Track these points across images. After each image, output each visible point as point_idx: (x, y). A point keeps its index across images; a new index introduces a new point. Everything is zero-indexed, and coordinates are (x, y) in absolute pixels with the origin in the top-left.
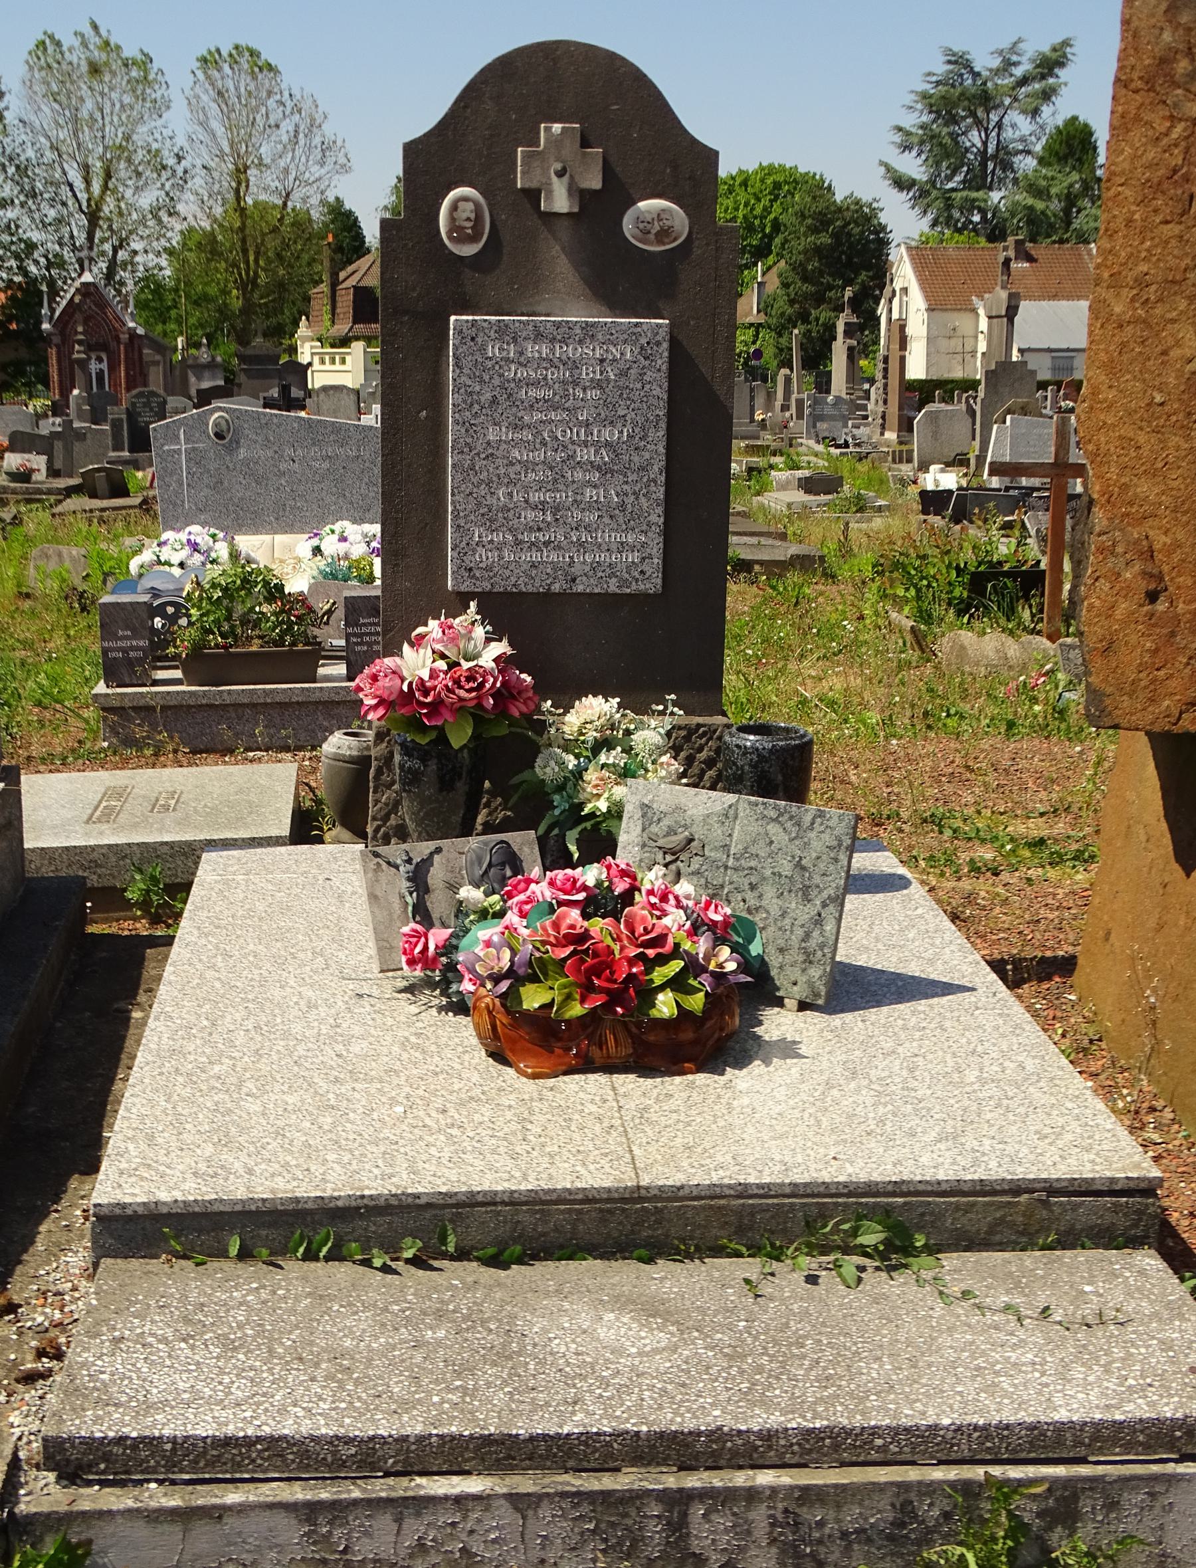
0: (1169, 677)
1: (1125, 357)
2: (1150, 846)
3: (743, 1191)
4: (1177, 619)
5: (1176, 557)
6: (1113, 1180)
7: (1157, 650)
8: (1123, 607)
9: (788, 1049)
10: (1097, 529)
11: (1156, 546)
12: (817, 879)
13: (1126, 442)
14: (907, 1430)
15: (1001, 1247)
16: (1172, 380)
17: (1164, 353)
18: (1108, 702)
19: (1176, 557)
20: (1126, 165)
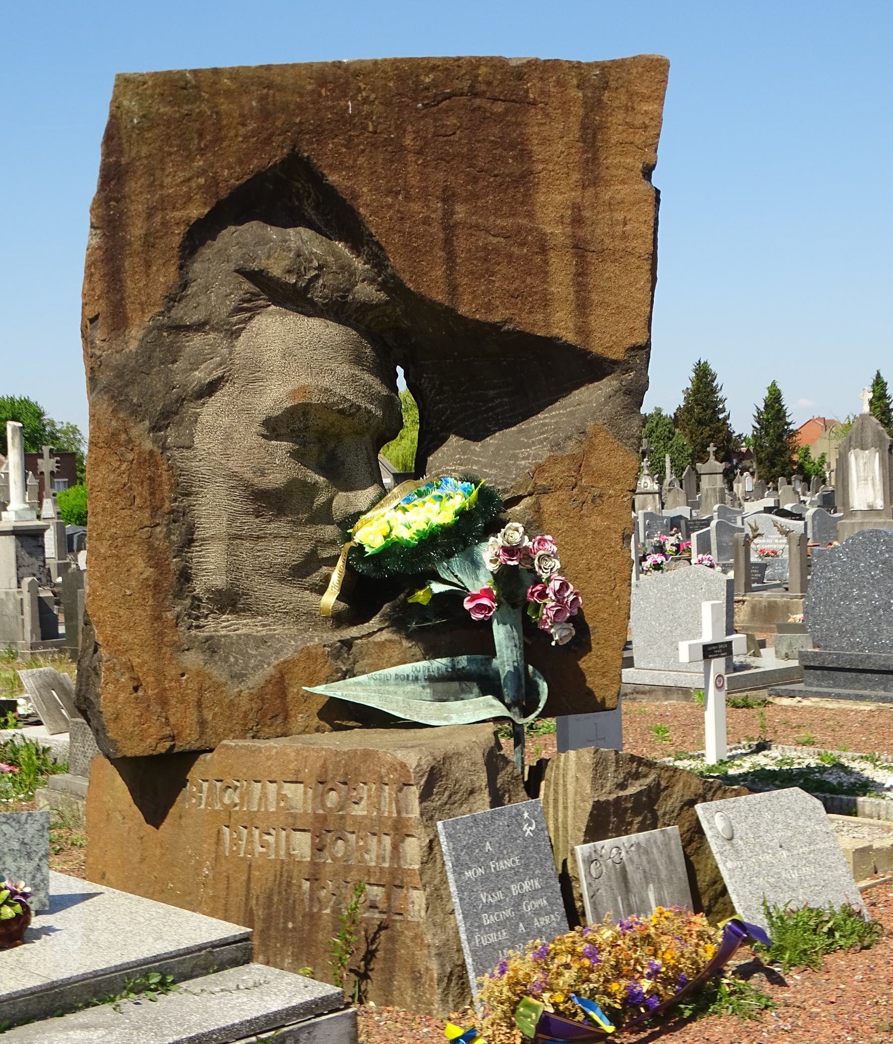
0: (149, 727)
1: (109, 574)
2: (126, 821)
3: (96, 974)
4: (149, 699)
5: (145, 669)
6: (235, 936)
7: (142, 715)
8: (122, 696)
9: (47, 930)
10: (105, 659)
11: (134, 664)
12: (34, 848)
13: (114, 615)
14: (224, 1029)
15: (197, 976)
16: (134, 583)
17: (128, 570)
18: (119, 745)
19: (145, 669)
20: (100, 482)
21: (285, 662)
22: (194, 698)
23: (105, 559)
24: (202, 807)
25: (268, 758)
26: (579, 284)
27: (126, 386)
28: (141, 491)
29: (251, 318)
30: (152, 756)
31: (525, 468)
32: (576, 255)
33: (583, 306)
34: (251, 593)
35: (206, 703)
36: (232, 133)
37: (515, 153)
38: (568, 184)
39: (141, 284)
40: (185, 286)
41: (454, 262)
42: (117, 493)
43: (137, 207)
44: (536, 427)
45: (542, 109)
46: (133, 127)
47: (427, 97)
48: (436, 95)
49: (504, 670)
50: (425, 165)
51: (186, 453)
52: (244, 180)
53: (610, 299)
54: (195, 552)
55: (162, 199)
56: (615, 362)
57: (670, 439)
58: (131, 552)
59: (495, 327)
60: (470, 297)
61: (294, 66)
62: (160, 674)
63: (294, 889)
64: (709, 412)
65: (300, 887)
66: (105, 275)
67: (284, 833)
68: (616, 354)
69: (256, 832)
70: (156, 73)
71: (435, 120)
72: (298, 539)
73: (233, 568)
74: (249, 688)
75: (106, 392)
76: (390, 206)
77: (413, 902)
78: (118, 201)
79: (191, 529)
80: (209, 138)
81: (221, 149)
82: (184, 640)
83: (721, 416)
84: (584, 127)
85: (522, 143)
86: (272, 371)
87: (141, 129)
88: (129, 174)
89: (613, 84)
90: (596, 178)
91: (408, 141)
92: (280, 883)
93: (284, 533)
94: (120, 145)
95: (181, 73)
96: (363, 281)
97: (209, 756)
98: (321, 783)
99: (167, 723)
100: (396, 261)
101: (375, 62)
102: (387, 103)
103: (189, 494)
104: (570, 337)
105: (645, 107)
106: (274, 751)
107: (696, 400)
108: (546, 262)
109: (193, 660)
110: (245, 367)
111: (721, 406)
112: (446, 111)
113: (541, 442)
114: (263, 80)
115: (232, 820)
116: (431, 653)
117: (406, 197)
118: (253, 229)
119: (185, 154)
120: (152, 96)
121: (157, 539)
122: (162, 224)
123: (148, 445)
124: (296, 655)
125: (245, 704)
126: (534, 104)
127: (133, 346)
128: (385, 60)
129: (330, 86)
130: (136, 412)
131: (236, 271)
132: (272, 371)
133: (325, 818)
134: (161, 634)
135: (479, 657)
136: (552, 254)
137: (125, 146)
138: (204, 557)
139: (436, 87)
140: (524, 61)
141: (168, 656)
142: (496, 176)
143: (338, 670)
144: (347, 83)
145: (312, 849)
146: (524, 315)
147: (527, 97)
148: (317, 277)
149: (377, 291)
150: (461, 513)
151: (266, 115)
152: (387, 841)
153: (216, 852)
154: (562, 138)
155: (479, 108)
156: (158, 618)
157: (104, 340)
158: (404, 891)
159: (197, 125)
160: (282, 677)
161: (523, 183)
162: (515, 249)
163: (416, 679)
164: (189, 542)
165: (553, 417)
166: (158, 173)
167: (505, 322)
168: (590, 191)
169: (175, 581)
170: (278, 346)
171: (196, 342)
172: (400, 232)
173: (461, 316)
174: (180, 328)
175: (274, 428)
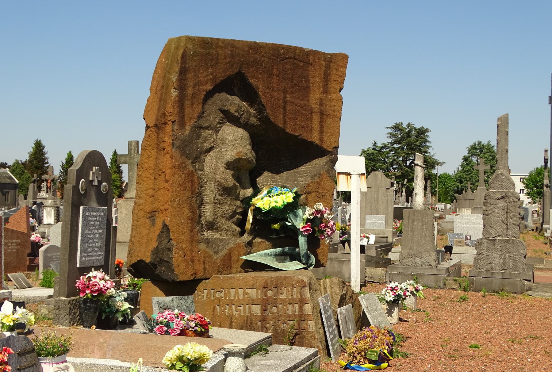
8: (180, 258)
22: (202, 260)
24: (205, 299)
25: (239, 280)
26: (321, 125)
27: (185, 147)
28: (189, 185)
29: (222, 126)
31: (302, 185)
32: (320, 115)
33: (321, 133)
35: (207, 262)
36: (222, 62)
40: (203, 113)
42: (181, 185)
43: (190, 83)
44: (301, 171)
50: (279, 80)
51: (202, 172)
53: (329, 131)
54: (203, 208)
55: (198, 81)
56: (329, 152)
57: (22, 175)
59: (296, 137)
61: (242, 41)
62: (192, 251)
63: (254, 325)
64: (41, 163)
65: (257, 324)
66: (179, 106)
67: (247, 306)
68: (330, 149)
69: (233, 307)
71: (283, 66)
72: (232, 205)
73: (214, 215)
76: (268, 93)
78: (184, 80)
79: (202, 199)
83: (46, 165)
84: (325, 74)
87: (193, 55)
89: (333, 61)
91: (274, 71)
92: (247, 323)
93: (229, 202)
94: (186, 61)
95: (207, 38)
97: (207, 281)
99: (194, 269)
100: (269, 111)
101: (267, 44)
102: (269, 58)
103: (202, 187)
104: (317, 142)
105: (342, 70)
107: (35, 157)
109: (202, 246)
110: (221, 143)
111: (46, 161)
112: (286, 63)
113: (305, 176)
114: (232, 44)
118: (224, 95)
120: (197, 45)
123: (191, 169)
125: (219, 263)
126: (311, 64)
127: (187, 133)
130: (188, 157)
133: (268, 300)
134: (193, 236)
136: (314, 114)
137: (188, 61)
143: (247, 251)
144: (258, 49)
145: (261, 311)
148: (243, 114)
150: (293, 198)
151: (232, 56)
152: (297, 306)
153: (213, 314)
156: (192, 231)
158: (306, 322)
159: (211, 57)
160: (230, 253)
161: (307, 89)
162: (304, 112)
163: (271, 255)
164: (201, 204)
165: (307, 168)
166: (197, 72)
167: (299, 135)
168: (325, 95)
169: (196, 218)
170: (232, 137)
171: (205, 133)
173: (287, 132)
174: (201, 128)
175: (229, 166)
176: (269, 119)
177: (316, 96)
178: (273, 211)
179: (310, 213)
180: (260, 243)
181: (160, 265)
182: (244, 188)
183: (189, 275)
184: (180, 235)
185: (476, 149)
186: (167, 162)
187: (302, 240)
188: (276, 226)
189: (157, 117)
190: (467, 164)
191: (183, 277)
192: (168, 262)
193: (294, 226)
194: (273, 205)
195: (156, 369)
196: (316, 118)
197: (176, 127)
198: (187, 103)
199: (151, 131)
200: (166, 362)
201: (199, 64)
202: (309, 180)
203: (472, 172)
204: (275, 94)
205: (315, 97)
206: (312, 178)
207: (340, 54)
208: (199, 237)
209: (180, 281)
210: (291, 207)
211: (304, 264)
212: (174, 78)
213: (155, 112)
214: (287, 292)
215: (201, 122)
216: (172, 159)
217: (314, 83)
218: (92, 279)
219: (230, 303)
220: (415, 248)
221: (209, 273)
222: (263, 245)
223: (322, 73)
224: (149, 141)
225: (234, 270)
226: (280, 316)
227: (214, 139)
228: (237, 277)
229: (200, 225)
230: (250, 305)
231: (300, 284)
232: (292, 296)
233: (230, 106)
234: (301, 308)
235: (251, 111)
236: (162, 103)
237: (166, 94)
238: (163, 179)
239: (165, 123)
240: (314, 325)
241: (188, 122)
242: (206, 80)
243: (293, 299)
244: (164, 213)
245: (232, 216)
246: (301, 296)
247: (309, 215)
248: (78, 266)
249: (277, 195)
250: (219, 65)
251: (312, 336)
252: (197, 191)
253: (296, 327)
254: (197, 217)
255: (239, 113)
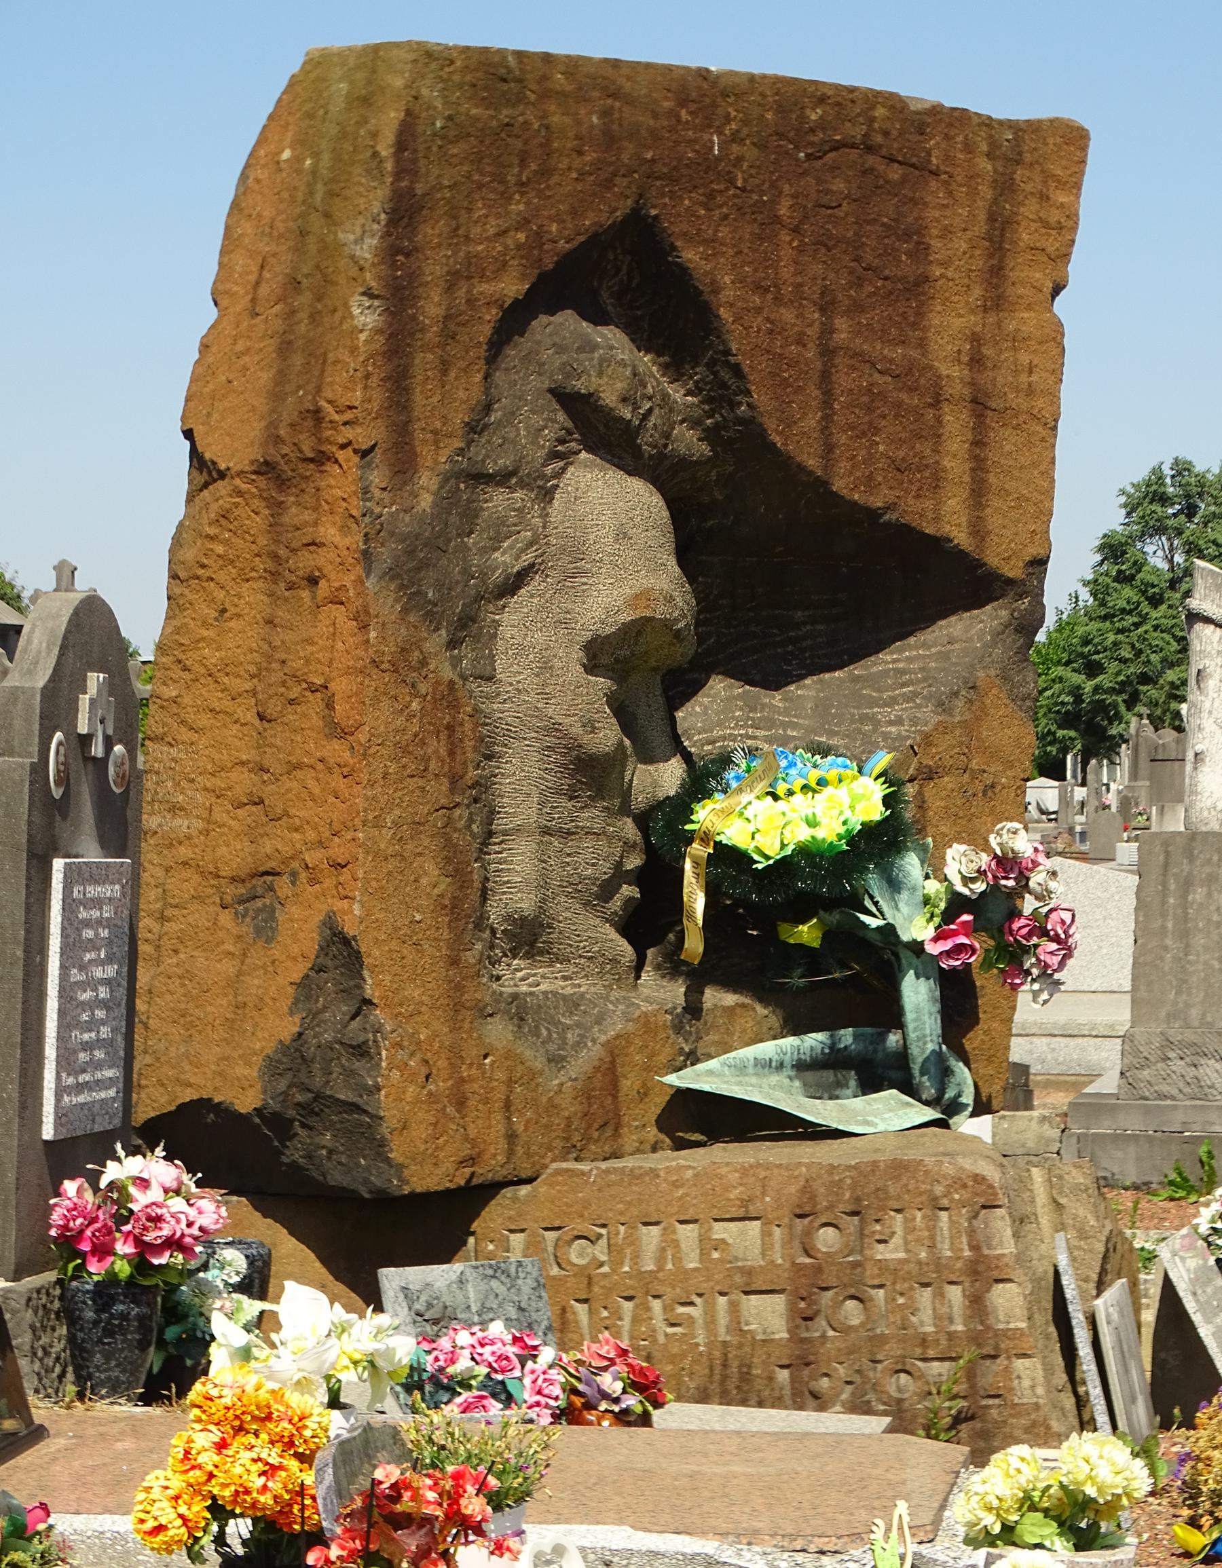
20: (382, 728)
21: (618, 1037)
22: (499, 1095)
23: (386, 859)
25: (676, 1185)
26: (976, 458)
27: (418, 569)
28: (437, 746)
29: (564, 470)
30: (448, 1191)
31: (900, 737)
33: (978, 493)
34: (556, 924)
35: (518, 1103)
37: (911, 246)
38: (967, 303)
39: (435, 399)
40: (488, 408)
41: (831, 408)
42: (406, 751)
43: (434, 269)
44: (886, 673)
45: (945, 182)
46: (435, 135)
47: (812, 144)
48: (824, 142)
49: (923, 1051)
50: (801, 250)
51: (487, 688)
52: (575, 244)
53: (1011, 485)
55: (469, 257)
56: (1010, 582)
58: (420, 850)
59: (873, 514)
60: (849, 465)
61: (648, 66)
62: (456, 1056)
63: (759, 1384)
65: (771, 1379)
67: (722, 1300)
68: (1013, 570)
69: (656, 1305)
70: (468, 48)
71: (819, 181)
72: (610, 838)
74: (571, 1079)
75: (392, 578)
76: (758, 310)
77: (1019, 1377)
78: (408, 255)
80: (533, 167)
81: (548, 187)
82: (488, 999)
84: (992, 218)
85: (918, 233)
86: (601, 560)
87: (442, 135)
88: (425, 212)
89: (1028, 157)
90: (999, 297)
92: (725, 1378)
93: (597, 826)
94: (415, 161)
95: (501, 52)
96: (682, 422)
97: (524, 1190)
98: (800, 1216)
101: (752, 78)
102: (762, 146)
103: (489, 757)
104: (961, 538)
105: (1062, 198)
106: (690, 1173)
108: (939, 420)
109: (498, 1031)
110: (563, 550)
113: (909, 698)
114: (604, 82)
115: (596, 1289)
116: (795, 1026)
117: (776, 298)
118: (568, 322)
119: (501, 188)
120: (460, 86)
121: (456, 830)
122: (468, 301)
123: (448, 673)
124: (631, 1027)
125: (570, 1106)
126: (936, 174)
127: (426, 502)
128: (764, 77)
129: (693, 107)
130: (432, 618)
131: (551, 391)
132: (601, 560)
133: (819, 1270)
134: (459, 988)
135: (869, 1030)
136: (946, 408)
138: (505, 862)
139: (824, 129)
140: (927, 106)
141: (467, 1025)
142: (886, 279)
144: (714, 105)
145: (791, 1319)
146: (910, 501)
147: (929, 161)
148: (650, 410)
149: (700, 440)
151: (610, 140)
152: (955, 1294)
154: (965, 230)
155: (872, 170)
156: (454, 962)
157: (384, 489)
158: (1002, 1361)
159: (518, 144)
160: (613, 1062)
161: (917, 289)
163: (781, 1066)
166: (463, 215)
171: (498, 501)
172: (768, 352)
173: (835, 495)
174: (480, 478)
175: (599, 654)
176: (762, 433)
177: (957, 322)
178: (805, 859)
179: (969, 870)
180: (730, 1011)
181: (311, 1121)
182: (648, 757)
183: (448, 1166)
184: (402, 983)
185: (1164, 500)
186: (331, 642)
187: (917, 995)
188: (807, 933)
189: (272, 425)
190: (1122, 578)
191: (427, 1177)
192: (356, 1108)
193: (889, 931)
194: (800, 834)
195: (800, 1557)
196: (956, 424)
197: (377, 477)
198: (423, 362)
199: (239, 493)
200: (982, 1514)
201: (469, 177)
202: (929, 717)
203: (1144, 618)
204: (788, 315)
205: (950, 323)
206: (942, 706)
207: (1054, 123)
208: (483, 991)
209: (413, 1196)
210: (878, 844)
211: (927, 1103)
212: (362, 241)
213: (261, 403)
214: (909, 1229)
215: (478, 452)
216: (364, 627)
217: (944, 264)
218: (132, 1190)
219: (642, 1289)
220: (1194, 1013)
221: (528, 1154)
222: (746, 1023)
223: (982, 216)
224: (226, 542)
225: (629, 1140)
226: (881, 1340)
227: (534, 530)
228: (668, 1170)
229: (487, 934)
230: (737, 1296)
231: (966, 1194)
232: (932, 1247)
233: (600, 374)
234: (977, 1304)
235: (677, 393)
236: (298, 360)
237: (314, 317)
238: (316, 721)
239: (321, 459)
240: (1040, 1373)
241: (425, 453)
242: (497, 249)
243: (938, 1264)
244: (329, 883)
245: (607, 890)
246: (975, 1248)
247: (966, 880)
248: (48, 1133)
249: (805, 788)
250: (555, 179)
251: (1034, 1424)
252: (472, 774)
253: (961, 1388)
254: (475, 897)
255: (636, 407)
